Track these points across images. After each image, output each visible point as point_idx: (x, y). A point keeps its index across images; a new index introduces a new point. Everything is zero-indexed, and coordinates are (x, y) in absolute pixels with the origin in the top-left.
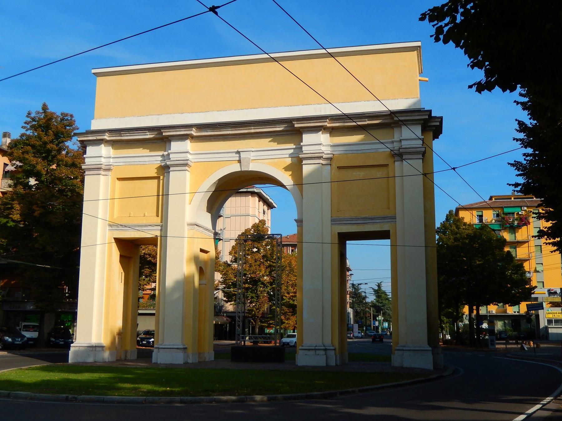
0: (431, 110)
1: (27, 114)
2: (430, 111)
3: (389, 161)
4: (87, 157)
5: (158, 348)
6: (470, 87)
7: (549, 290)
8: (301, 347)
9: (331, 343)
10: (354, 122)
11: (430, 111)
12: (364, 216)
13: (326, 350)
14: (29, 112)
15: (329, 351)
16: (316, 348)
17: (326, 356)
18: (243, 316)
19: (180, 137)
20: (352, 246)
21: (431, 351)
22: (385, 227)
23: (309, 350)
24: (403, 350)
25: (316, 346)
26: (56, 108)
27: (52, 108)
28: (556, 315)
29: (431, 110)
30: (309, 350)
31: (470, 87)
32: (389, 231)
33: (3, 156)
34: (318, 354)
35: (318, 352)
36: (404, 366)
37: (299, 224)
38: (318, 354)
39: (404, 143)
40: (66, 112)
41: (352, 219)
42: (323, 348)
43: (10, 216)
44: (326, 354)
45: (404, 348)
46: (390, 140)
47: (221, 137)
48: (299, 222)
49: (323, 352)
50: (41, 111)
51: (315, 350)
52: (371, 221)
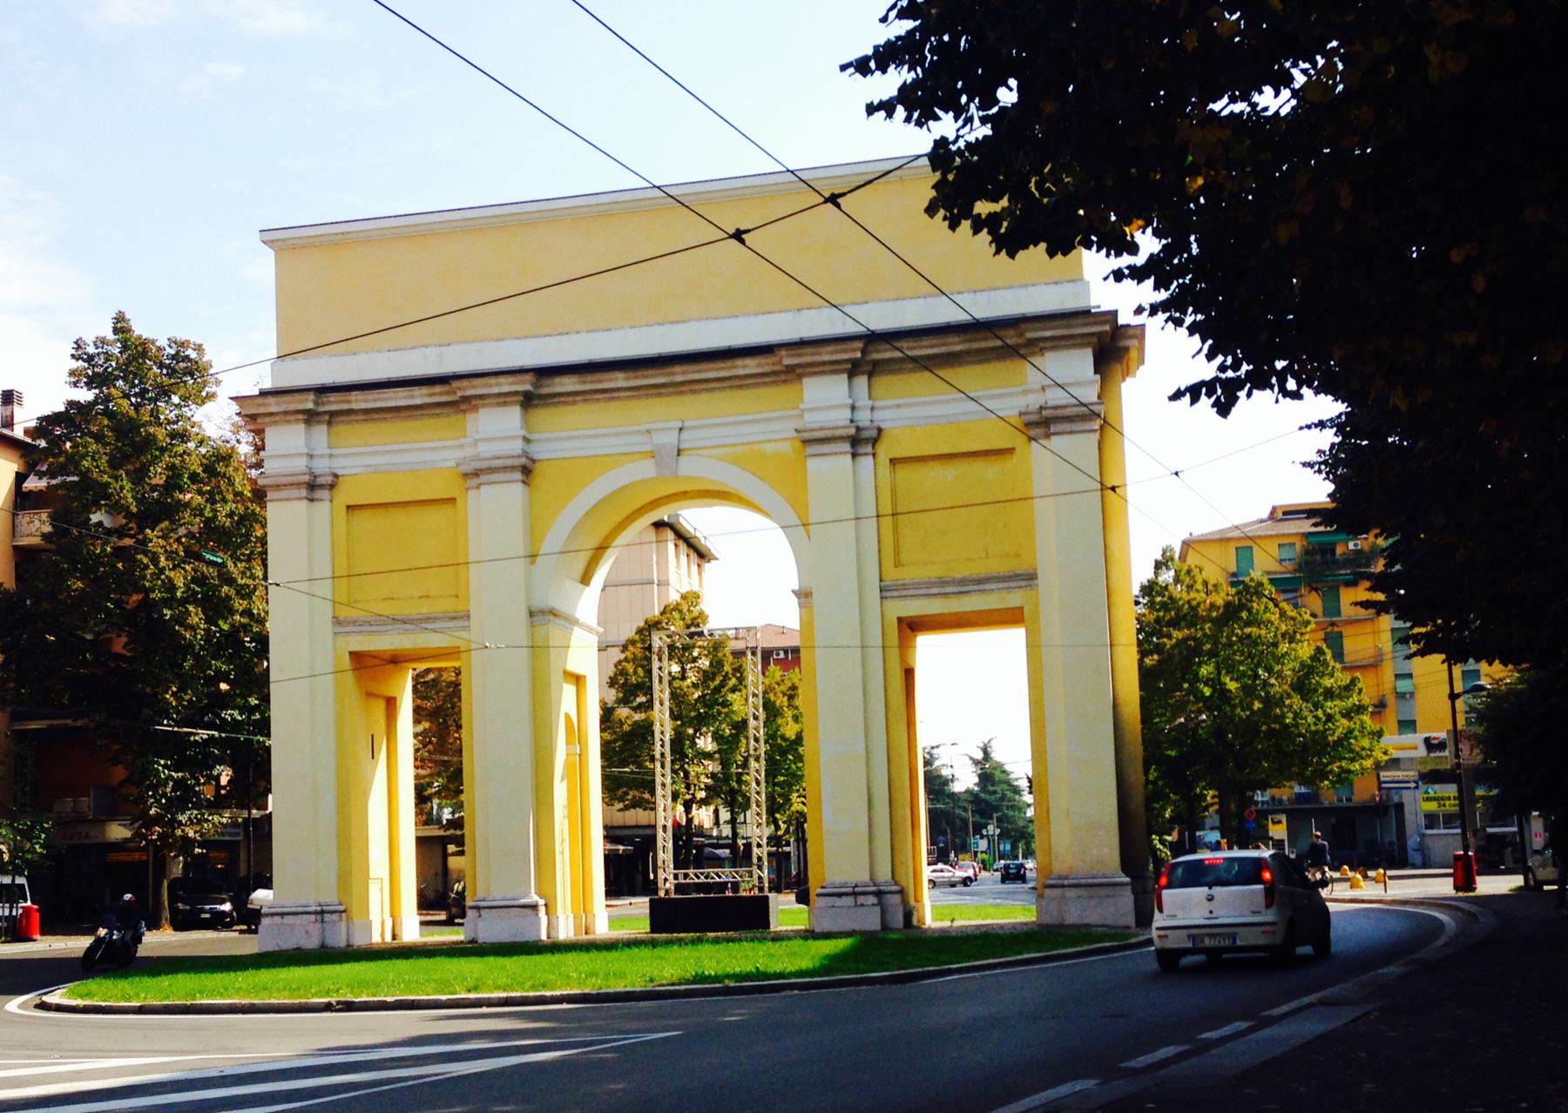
0: (1116, 311)
1: (73, 352)
2: (1114, 313)
3: (1017, 440)
4: (272, 457)
5: (478, 908)
6: (1106, 279)
7: (1427, 740)
8: (820, 891)
9: (890, 876)
10: (897, 349)
11: (1114, 313)
12: (958, 575)
13: (879, 894)
14: (76, 343)
15: (889, 896)
16: (856, 889)
17: (882, 908)
18: (676, 825)
19: (502, 400)
20: (927, 646)
21: (1130, 887)
22: (1014, 599)
23: (840, 895)
24: (1063, 886)
25: (856, 886)
26: (154, 328)
27: (141, 328)
28: (1447, 803)
29: (1116, 311)
30: (840, 895)
31: (1106, 279)
32: (1021, 609)
33: (1319, 393)
34: (862, 905)
35: (861, 899)
36: (1067, 923)
37: (803, 600)
38: (862, 905)
39: (808, 417)
40: (182, 337)
41: (932, 584)
42: (873, 889)
43: (1187, 163)
44: (880, 903)
45: (1066, 882)
46: (1019, 389)
47: (601, 396)
48: (803, 595)
49: (872, 900)
50: (111, 336)
51: (855, 894)
52: (977, 587)
